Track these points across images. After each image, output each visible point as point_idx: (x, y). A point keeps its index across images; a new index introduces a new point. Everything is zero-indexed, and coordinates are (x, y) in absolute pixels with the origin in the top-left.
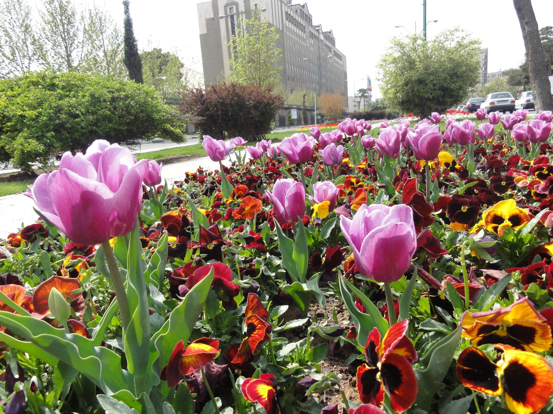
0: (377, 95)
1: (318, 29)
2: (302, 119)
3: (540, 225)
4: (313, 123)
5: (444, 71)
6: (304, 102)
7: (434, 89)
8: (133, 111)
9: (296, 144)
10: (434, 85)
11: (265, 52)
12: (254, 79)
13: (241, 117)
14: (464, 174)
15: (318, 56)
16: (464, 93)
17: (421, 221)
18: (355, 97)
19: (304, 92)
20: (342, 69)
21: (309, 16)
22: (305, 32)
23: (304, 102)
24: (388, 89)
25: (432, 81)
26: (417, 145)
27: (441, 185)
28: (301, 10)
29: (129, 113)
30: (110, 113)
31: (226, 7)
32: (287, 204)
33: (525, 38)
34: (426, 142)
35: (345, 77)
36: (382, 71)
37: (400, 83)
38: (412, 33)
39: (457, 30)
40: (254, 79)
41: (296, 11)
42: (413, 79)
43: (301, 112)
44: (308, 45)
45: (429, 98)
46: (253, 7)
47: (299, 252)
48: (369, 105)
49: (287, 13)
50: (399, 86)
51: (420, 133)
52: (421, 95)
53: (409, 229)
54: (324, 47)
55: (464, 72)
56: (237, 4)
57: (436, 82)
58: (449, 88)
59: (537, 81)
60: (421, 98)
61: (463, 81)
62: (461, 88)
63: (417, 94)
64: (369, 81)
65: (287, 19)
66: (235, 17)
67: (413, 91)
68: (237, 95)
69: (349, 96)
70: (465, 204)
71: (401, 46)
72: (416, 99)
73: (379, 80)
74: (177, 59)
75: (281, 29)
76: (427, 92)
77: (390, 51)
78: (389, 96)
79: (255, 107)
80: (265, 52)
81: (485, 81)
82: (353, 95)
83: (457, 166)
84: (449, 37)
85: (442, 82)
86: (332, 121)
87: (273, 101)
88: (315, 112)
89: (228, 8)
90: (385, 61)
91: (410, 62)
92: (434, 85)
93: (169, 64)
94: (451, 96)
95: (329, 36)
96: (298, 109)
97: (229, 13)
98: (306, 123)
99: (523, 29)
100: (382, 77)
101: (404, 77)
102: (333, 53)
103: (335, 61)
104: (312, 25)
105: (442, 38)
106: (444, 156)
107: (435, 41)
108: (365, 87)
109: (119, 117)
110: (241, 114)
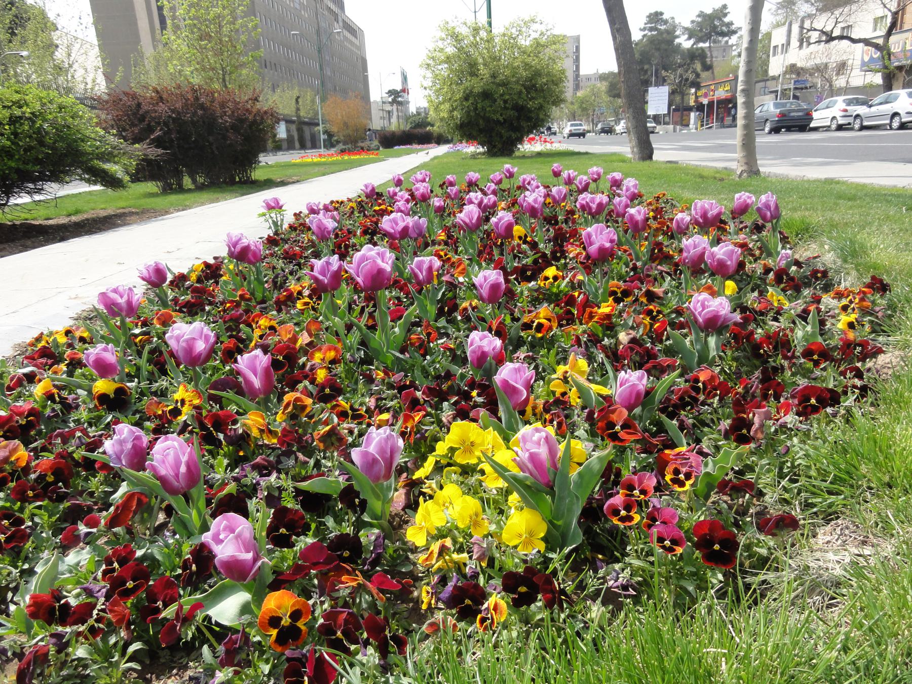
0: (418, 100)
2: (296, 137)
3: (571, 281)
4: (314, 146)
5: (517, 82)
6: (298, 109)
7: (505, 108)
8: (48, 140)
9: (397, 224)
10: (505, 102)
11: (229, 23)
12: (213, 69)
13: (211, 144)
14: (534, 245)
15: (316, 27)
16: (545, 115)
17: (507, 281)
18: (384, 103)
19: (296, 93)
20: (359, 52)
23: (298, 109)
24: (440, 103)
25: (502, 95)
26: (497, 228)
27: (515, 256)
29: (41, 143)
30: (9, 143)
32: (424, 273)
33: (616, 50)
34: (504, 226)
35: (365, 69)
36: (429, 74)
37: (458, 97)
38: (470, 20)
39: (533, 21)
40: (213, 69)
42: (476, 90)
43: (293, 127)
44: (298, 6)
45: (498, 121)
47: (432, 304)
48: (407, 118)
50: (456, 101)
51: (500, 220)
52: (487, 115)
53: (502, 280)
54: (326, 12)
55: (545, 85)
57: (507, 97)
58: (526, 106)
59: (631, 110)
60: (488, 120)
61: (544, 98)
62: (541, 107)
63: (482, 114)
64: (405, 78)
67: (476, 109)
68: (202, 107)
69: (372, 100)
70: (529, 270)
71: (456, 37)
72: (481, 122)
73: (425, 88)
74: (43, 14)
76: (495, 112)
77: (440, 44)
78: (442, 115)
79: (234, 127)
80: (229, 23)
81: (577, 87)
82: (379, 99)
83: (529, 239)
84: (524, 29)
85: (515, 97)
86: (350, 146)
87: (262, 118)
88: (321, 128)
90: (433, 58)
91: (470, 64)
92: (505, 102)
93: (30, 25)
94: (529, 119)
96: (288, 122)
98: (303, 147)
99: (614, 38)
100: (430, 84)
101: (462, 87)
102: (341, 23)
103: (346, 38)
105: (514, 31)
106: (518, 231)
107: (504, 35)
108: (399, 87)
109: (26, 150)
110: (211, 139)
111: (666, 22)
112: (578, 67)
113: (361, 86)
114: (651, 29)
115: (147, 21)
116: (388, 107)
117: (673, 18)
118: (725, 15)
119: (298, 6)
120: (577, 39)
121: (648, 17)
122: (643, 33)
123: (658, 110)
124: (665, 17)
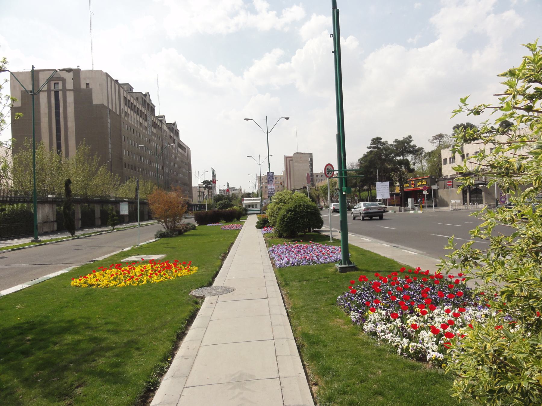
1: (161, 119)
21: (151, 105)
22: (146, 121)
28: (142, 98)
31: (49, 81)
41: (137, 98)
44: (150, 134)
46: (83, 86)
49: (125, 98)
54: (168, 138)
56: (64, 80)
64: (213, 174)
65: (126, 104)
66: (61, 94)
69: (193, 185)
75: (118, 113)
82: (197, 185)
89: (52, 83)
95: (173, 128)
97: (53, 88)
102: (176, 144)
103: (180, 153)
104: (154, 115)
108: (210, 179)
111: (383, 144)
112: (312, 170)
113: (187, 178)
114: (374, 148)
115: (48, 139)
116: (203, 190)
117: (387, 142)
118: (411, 141)
119: (150, 134)
120: (311, 155)
121: (372, 140)
122: (369, 150)
123: (383, 196)
124: (383, 141)
